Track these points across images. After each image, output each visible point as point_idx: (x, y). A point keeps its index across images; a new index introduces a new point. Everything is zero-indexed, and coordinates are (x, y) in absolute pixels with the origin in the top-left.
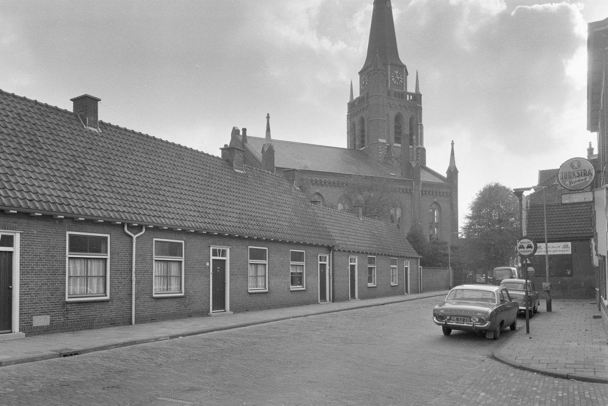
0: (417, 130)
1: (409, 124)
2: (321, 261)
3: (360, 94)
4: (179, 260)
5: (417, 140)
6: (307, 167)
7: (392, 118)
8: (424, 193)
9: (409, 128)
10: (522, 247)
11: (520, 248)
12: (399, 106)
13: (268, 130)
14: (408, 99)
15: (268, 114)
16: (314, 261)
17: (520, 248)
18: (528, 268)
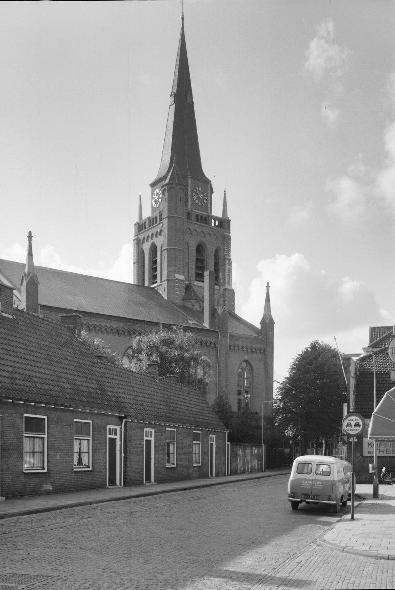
0: (225, 265)
1: (213, 257)
2: (110, 434)
3: (152, 214)
4: (79, 438)
5: (224, 278)
6: (82, 307)
7: (193, 248)
8: (232, 348)
10: (349, 425)
14: (213, 225)
15: (30, 233)
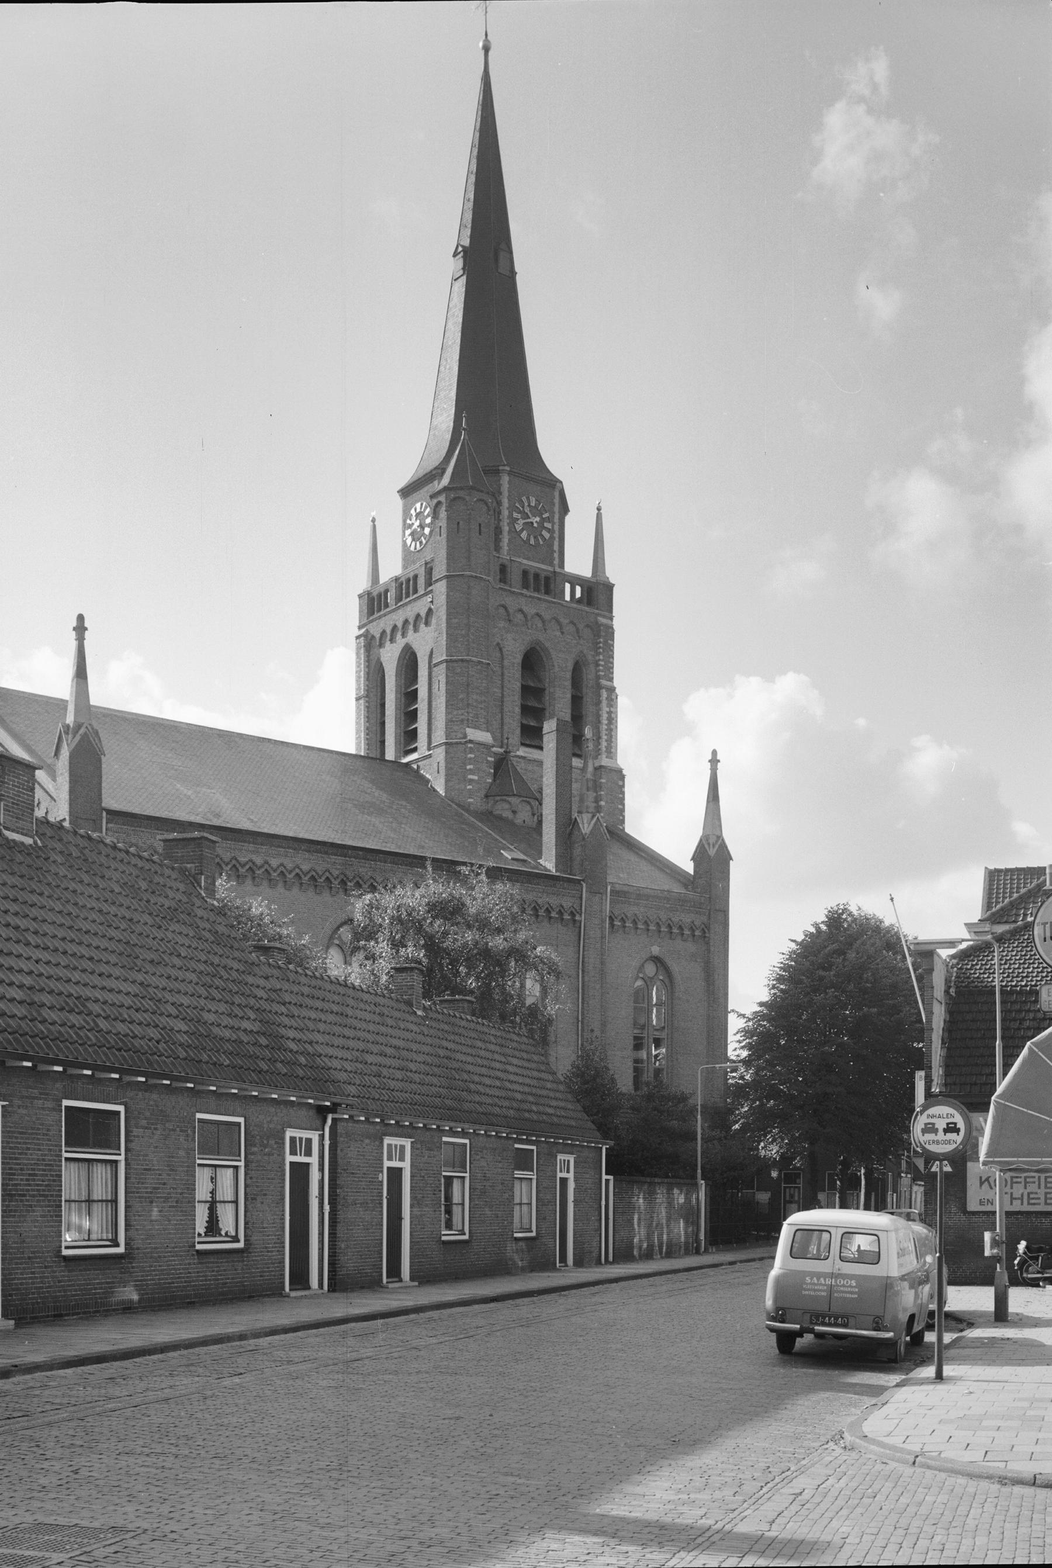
0: (598, 703)
2: (293, 1152)
3: (405, 567)
6: (218, 816)
8: (617, 923)
9: (569, 696)
10: (930, 1129)
11: (925, 1131)
12: (537, 620)
13: (81, 673)
14: (568, 598)
15: (81, 618)
16: (269, 1154)
17: (925, 1131)
18: (624, 1090)
